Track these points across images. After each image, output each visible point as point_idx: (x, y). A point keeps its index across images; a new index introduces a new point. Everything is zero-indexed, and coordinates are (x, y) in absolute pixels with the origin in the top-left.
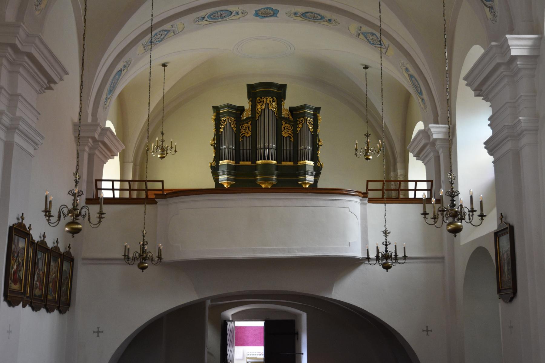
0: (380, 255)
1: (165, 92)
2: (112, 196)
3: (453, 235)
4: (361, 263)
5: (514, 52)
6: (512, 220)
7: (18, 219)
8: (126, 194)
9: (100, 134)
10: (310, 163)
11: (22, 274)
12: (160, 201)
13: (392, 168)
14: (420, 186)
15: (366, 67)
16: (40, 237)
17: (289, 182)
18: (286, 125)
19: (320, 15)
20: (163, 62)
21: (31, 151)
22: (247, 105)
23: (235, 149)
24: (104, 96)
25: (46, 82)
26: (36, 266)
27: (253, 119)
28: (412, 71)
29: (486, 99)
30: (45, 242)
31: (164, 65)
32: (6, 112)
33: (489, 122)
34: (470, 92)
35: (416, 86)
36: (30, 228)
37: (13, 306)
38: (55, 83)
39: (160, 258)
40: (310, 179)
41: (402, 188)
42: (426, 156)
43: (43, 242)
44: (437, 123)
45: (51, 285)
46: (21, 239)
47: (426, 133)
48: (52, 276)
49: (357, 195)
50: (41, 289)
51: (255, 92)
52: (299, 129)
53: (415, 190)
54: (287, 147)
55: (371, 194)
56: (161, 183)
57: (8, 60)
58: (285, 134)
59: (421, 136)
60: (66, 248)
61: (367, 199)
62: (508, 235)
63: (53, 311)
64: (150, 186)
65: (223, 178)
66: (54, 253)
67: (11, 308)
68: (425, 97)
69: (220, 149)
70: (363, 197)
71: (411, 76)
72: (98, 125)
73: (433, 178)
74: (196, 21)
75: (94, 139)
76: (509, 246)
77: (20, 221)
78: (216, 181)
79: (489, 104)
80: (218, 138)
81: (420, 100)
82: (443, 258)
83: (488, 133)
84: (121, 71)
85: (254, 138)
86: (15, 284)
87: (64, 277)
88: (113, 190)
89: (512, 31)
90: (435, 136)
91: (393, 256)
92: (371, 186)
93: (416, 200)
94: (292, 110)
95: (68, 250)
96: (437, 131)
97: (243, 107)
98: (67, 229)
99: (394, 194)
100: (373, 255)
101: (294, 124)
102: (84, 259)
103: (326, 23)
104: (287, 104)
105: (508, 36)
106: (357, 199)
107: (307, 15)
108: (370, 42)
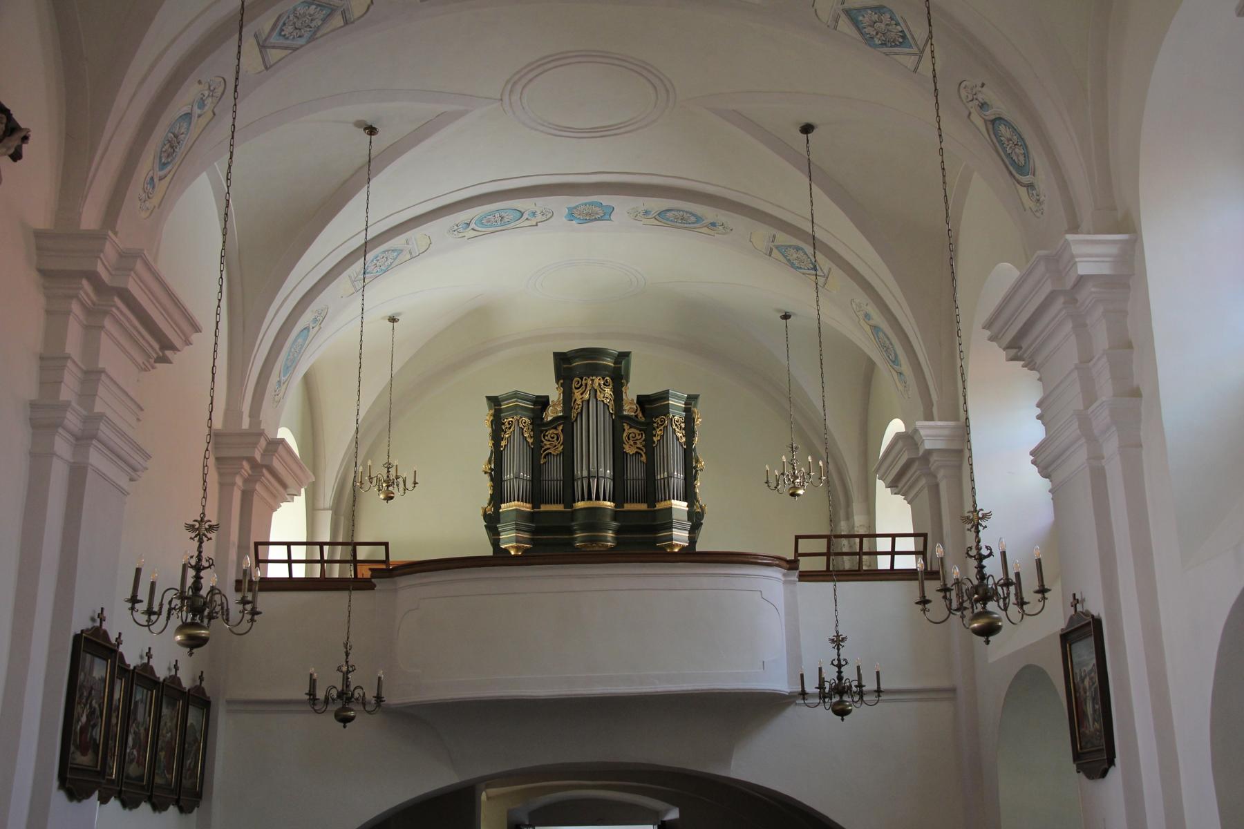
0: (827, 685)
1: (395, 370)
2: (287, 576)
3: (983, 639)
4: (789, 704)
5: (1083, 269)
6: (1095, 606)
7: (93, 620)
8: (316, 572)
9: (265, 451)
10: (680, 506)
11: (98, 733)
12: (380, 584)
13: (842, 513)
14: (901, 544)
15: (786, 317)
16: (141, 657)
17: (643, 540)
18: (633, 430)
19: (693, 215)
20: (390, 314)
21: (123, 482)
22: (554, 393)
23: (532, 480)
24: (274, 379)
25: (157, 346)
26: (132, 717)
27: (566, 421)
28: (878, 318)
29: (1031, 365)
30: (152, 668)
31: (393, 320)
32: (74, 404)
33: (1038, 411)
34: (998, 354)
35: (886, 349)
36: (119, 640)
37: (80, 801)
38: (173, 348)
39: (379, 698)
40: (680, 536)
41: (865, 549)
42: (911, 487)
43: (147, 668)
44: (932, 420)
45: (162, 754)
46: (97, 660)
47: (907, 439)
48: (166, 735)
49: (777, 566)
50: (141, 764)
51: (571, 366)
52: (655, 439)
53: (893, 553)
54: (635, 472)
55: (805, 564)
56: (383, 547)
57: (83, 305)
58: (629, 449)
59: (900, 444)
60: (194, 680)
61: (797, 573)
62: (1091, 640)
63: (166, 809)
64: (363, 553)
65: (509, 539)
66: (169, 690)
67: (75, 803)
68: (905, 367)
69: (502, 481)
70: (789, 569)
71: (875, 329)
72: (261, 434)
73: (927, 529)
74: (455, 230)
75: (251, 460)
76: (1094, 661)
77: (98, 624)
78: (495, 543)
79: (1036, 374)
80: (498, 457)
81: (895, 374)
82: (953, 690)
83: (1036, 433)
84: (307, 329)
85: (568, 457)
86: (84, 753)
87: (189, 739)
88: (290, 561)
89: (1075, 228)
90: (928, 445)
91: (854, 689)
92: (804, 546)
93: (893, 574)
94: (643, 401)
95: (198, 683)
96: (933, 435)
97: (547, 398)
98: (179, 638)
99: (847, 563)
100: (811, 687)
101: (647, 428)
102: (229, 702)
103: (705, 230)
104: (631, 393)
105: (1069, 237)
106: (777, 574)
107: (669, 214)
108: (792, 265)
